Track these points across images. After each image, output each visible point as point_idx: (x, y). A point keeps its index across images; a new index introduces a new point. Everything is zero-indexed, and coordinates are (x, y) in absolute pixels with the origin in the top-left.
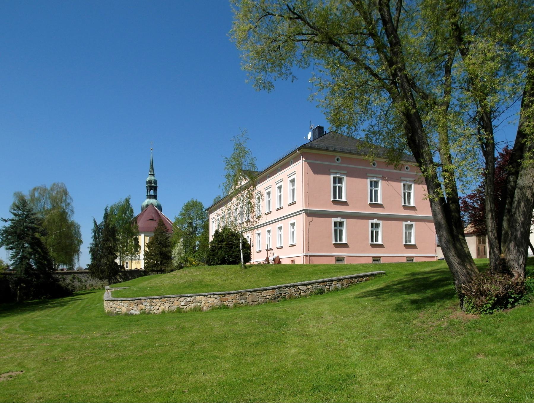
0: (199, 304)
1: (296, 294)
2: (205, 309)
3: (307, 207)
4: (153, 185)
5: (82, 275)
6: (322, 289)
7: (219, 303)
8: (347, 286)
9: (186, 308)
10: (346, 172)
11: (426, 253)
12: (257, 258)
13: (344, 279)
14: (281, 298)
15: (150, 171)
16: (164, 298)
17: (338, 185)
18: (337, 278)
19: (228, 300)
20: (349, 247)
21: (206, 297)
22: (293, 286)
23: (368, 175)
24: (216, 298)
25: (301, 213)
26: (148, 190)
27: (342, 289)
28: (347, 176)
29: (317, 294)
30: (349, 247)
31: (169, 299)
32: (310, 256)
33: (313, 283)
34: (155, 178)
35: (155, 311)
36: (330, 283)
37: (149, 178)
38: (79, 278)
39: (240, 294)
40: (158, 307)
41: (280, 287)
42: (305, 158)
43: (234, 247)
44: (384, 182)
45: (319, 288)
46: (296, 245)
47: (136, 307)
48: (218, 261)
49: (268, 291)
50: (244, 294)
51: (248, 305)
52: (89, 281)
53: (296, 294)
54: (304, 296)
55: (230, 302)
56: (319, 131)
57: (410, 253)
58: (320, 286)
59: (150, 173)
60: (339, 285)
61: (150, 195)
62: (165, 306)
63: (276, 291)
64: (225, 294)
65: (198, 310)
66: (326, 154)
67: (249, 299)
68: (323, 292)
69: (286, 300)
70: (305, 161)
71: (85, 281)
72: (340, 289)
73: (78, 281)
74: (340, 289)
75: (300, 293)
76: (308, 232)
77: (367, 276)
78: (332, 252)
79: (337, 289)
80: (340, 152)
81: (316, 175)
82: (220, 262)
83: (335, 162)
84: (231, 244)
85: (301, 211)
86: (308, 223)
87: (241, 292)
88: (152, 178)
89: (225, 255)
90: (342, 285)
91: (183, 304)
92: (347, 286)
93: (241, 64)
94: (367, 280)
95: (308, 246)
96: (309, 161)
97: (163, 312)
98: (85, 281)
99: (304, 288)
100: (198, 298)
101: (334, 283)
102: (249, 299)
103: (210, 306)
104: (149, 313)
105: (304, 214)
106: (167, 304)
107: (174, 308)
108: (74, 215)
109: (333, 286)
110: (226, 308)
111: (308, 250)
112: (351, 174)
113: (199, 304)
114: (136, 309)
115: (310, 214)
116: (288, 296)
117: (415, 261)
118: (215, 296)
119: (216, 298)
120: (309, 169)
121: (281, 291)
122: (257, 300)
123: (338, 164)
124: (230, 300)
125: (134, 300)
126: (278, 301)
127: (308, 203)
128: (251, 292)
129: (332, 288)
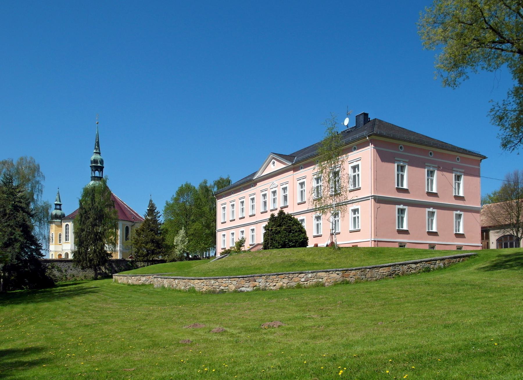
0: (321, 280)
1: (407, 272)
2: (327, 284)
3: (376, 194)
4: (99, 165)
5: (62, 264)
6: (429, 268)
7: (341, 279)
8: (448, 265)
9: (307, 284)
10: (407, 161)
11: (472, 242)
12: (311, 245)
13: (446, 259)
14: (396, 274)
15: (95, 149)
16: (282, 274)
17: (400, 173)
18: (440, 257)
19: (350, 276)
20: (410, 234)
21: (328, 273)
22: (405, 264)
23: (426, 164)
24: (338, 274)
25: (369, 199)
26: (92, 170)
27: (445, 268)
28: (409, 165)
29: (424, 272)
30: (410, 234)
31: (287, 275)
32: (378, 241)
33: (421, 262)
34: (101, 157)
35: (271, 288)
36: (435, 262)
37: (93, 157)
38: (58, 267)
39: (360, 270)
40: (275, 284)
41: (395, 265)
42: (374, 145)
43: (292, 231)
44: (439, 172)
45: (426, 266)
46: (360, 231)
47: (247, 284)
48: (279, 245)
49: (384, 268)
50: (364, 270)
51: (367, 280)
52: (69, 271)
53: (407, 272)
54: (414, 273)
55: (351, 277)
56: (364, 117)
57: (459, 242)
58: (427, 265)
59: (95, 151)
60: (441, 264)
61: (95, 177)
62: (283, 282)
63: (391, 268)
64: (347, 270)
65: (319, 285)
66: (383, 140)
67: (369, 275)
68: (429, 270)
69: (399, 276)
70: (374, 148)
71: (66, 271)
72: (443, 268)
73: (58, 271)
74: (443, 268)
75: (411, 270)
76: (376, 218)
77: (464, 257)
78: (396, 238)
79: (440, 268)
80: (405, 141)
81: (383, 163)
82: (280, 246)
83: (399, 151)
84: (290, 228)
85: (369, 197)
86: (376, 209)
87: (362, 269)
88: (98, 157)
89: (286, 239)
90: (444, 264)
91: (303, 280)
92: (448, 265)
93: (435, 63)
94: (463, 260)
95: (377, 231)
96: (377, 148)
97: (281, 288)
98: (66, 271)
99: (414, 266)
100: (319, 274)
101: (437, 262)
102: (369, 275)
103: (332, 281)
104: (264, 290)
105: (373, 200)
106: (286, 281)
107: (294, 284)
108: (43, 196)
109: (437, 265)
110: (348, 283)
111: (376, 235)
112: (412, 163)
113: (321, 280)
114: (248, 286)
115: (379, 200)
116: (401, 273)
117: (463, 249)
118: (337, 272)
119: (338, 274)
120: (378, 155)
121: (395, 268)
122: (376, 276)
123: (401, 152)
124: (352, 276)
125: (246, 277)
126: (393, 278)
127: (376, 189)
128: (370, 268)
129: (436, 266)
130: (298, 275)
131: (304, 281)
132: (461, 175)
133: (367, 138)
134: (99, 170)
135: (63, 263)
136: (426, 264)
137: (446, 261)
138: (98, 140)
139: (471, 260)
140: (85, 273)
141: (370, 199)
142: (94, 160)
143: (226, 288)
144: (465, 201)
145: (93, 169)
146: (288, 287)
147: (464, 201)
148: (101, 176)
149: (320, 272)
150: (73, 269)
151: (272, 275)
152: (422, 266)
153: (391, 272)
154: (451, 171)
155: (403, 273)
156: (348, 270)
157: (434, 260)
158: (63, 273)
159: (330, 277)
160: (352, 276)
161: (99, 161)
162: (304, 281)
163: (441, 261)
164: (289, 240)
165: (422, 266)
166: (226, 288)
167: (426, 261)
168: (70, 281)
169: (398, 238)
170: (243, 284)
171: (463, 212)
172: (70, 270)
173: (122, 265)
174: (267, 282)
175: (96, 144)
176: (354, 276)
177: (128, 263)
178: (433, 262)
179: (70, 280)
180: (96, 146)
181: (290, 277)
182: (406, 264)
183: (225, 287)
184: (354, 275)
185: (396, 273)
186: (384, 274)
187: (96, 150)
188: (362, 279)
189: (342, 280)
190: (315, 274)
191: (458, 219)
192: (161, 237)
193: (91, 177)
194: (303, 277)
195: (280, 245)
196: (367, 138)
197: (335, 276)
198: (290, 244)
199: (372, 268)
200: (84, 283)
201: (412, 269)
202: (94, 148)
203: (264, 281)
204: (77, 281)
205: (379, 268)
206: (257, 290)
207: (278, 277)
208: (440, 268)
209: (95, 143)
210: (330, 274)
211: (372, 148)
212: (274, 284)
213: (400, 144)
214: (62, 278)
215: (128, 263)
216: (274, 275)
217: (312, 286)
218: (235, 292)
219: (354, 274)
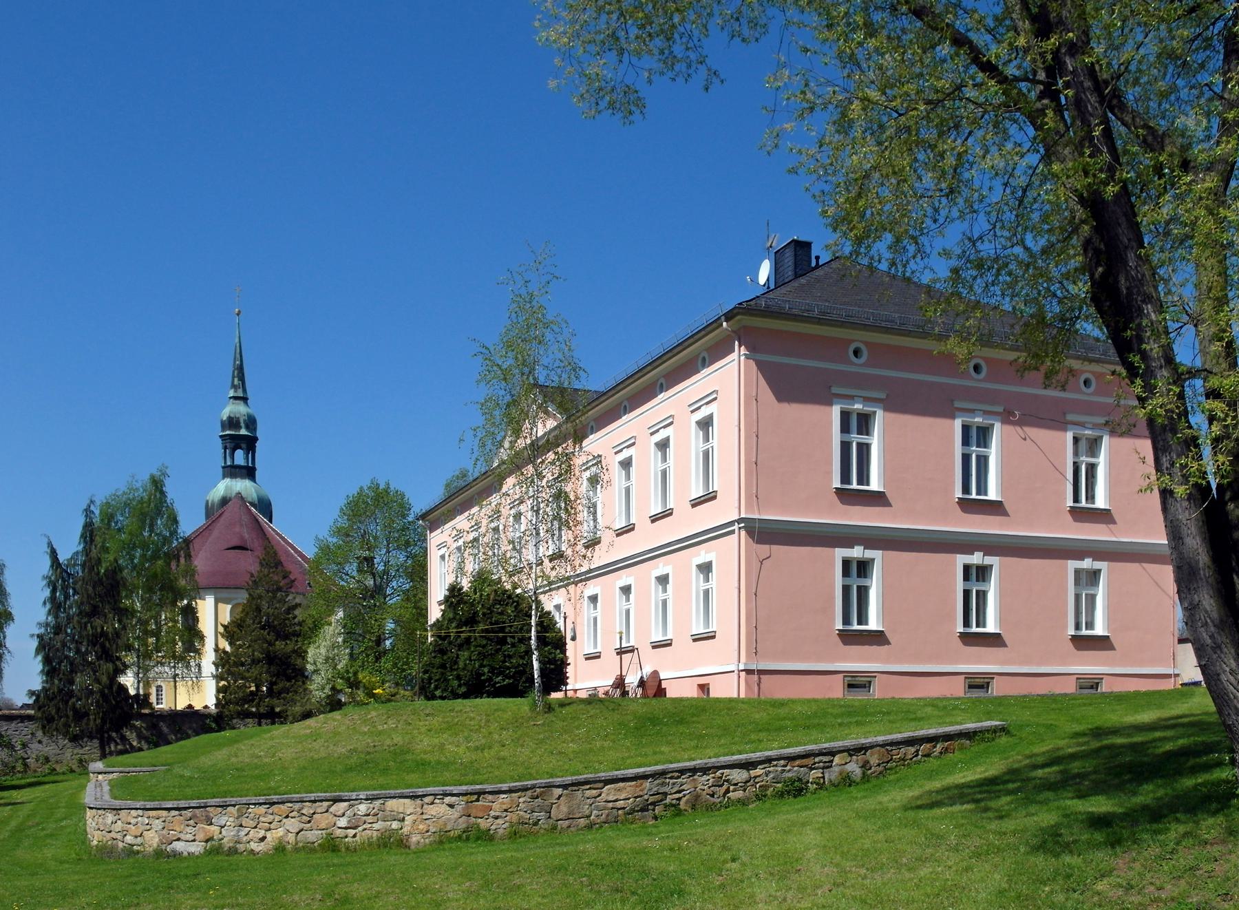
0: (395, 825)
1: (712, 796)
2: (414, 839)
3: (753, 513)
4: (243, 432)
8: (881, 768)
9: (355, 836)
10: (883, 396)
14: (666, 806)
15: (234, 387)
16: (283, 803)
18: (848, 743)
19: (492, 813)
20: (889, 643)
21: (418, 801)
22: (705, 770)
23: (957, 404)
24: (451, 806)
25: (733, 532)
27: (865, 778)
28: (886, 409)
29: (781, 795)
30: (889, 643)
31: (297, 806)
32: (761, 672)
33: (769, 760)
34: (250, 411)
35: (253, 846)
36: (826, 759)
39: (529, 793)
40: (262, 833)
41: (663, 774)
42: (747, 348)
43: (509, 640)
44: (1010, 429)
45: (790, 775)
47: (189, 829)
48: (460, 686)
49: (621, 784)
50: (541, 794)
51: (554, 828)
52: (35, 746)
53: (712, 796)
54: (739, 800)
55: (497, 818)
58: (793, 771)
59: (232, 393)
60: (854, 768)
61: (233, 467)
63: (647, 784)
64: (480, 793)
65: (393, 842)
67: (560, 810)
68: (801, 790)
69: (679, 813)
70: (747, 357)
71: (24, 746)
75: (728, 791)
76: (754, 594)
77: (948, 737)
80: (865, 327)
85: (731, 523)
86: (756, 565)
87: (533, 787)
88: (240, 409)
90: (865, 765)
91: (343, 822)
93: (537, 24)
94: (945, 751)
97: (280, 848)
98: (24, 746)
99: (738, 775)
100: (392, 804)
101: (837, 760)
102: (560, 810)
104: (233, 851)
105: (743, 533)
106: (293, 824)
107: (313, 836)
110: (486, 837)
111: (755, 652)
112: (901, 401)
113: (395, 825)
114: (190, 837)
116: (687, 802)
118: (448, 800)
120: (762, 382)
121: (663, 784)
122: (587, 813)
125: (185, 809)
127: (754, 496)
128: (565, 787)
129: (832, 775)
130: (330, 807)
131: (346, 828)
132: (1102, 437)
133: (725, 324)
134: (244, 446)
135: (15, 722)
136: (788, 768)
137: (872, 755)
138: (241, 360)
139: (977, 748)
140: (81, 751)
141: (737, 531)
142: (230, 418)
143: (139, 840)
144: (1114, 522)
145: (228, 445)
146: (301, 845)
147: (1111, 526)
148: (250, 465)
149: (394, 797)
150: (45, 740)
151: (255, 804)
152: (771, 776)
153: (646, 797)
154: (1060, 424)
155: (695, 803)
156: (485, 793)
157: (821, 753)
158: (15, 751)
159: (425, 817)
160: (497, 814)
161: (242, 421)
162: (346, 828)
163: (851, 755)
164: (492, 670)
165: (771, 776)
166: (139, 840)
167: (791, 759)
168: (37, 775)
169: (845, 659)
170: (178, 829)
171: (1106, 563)
172: (37, 744)
173: (190, 728)
174: (241, 826)
175: (236, 372)
176: (505, 814)
177: (208, 721)
178: (817, 760)
179: (35, 771)
180: (236, 380)
181: (304, 811)
182: (709, 769)
183: (136, 837)
184: (506, 810)
185: (668, 801)
186: (620, 804)
187: (235, 392)
188: (536, 824)
189: (464, 826)
190: (377, 803)
191: (1092, 585)
192: (291, 646)
193: (223, 468)
194: (344, 815)
195: (464, 684)
196: (725, 324)
197: (443, 813)
198: (497, 680)
199: (573, 784)
200: (48, 783)
201: (732, 788)
202: (230, 384)
203: (233, 824)
204: (57, 774)
205: (600, 785)
206: (215, 850)
207: (270, 811)
208: (847, 781)
209: (231, 369)
210: (425, 806)
211: (742, 358)
212: (261, 835)
213: (853, 341)
214: (14, 767)
215: (208, 721)
216: (261, 804)
217: (370, 844)
218: (159, 854)
219: (505, 807)
